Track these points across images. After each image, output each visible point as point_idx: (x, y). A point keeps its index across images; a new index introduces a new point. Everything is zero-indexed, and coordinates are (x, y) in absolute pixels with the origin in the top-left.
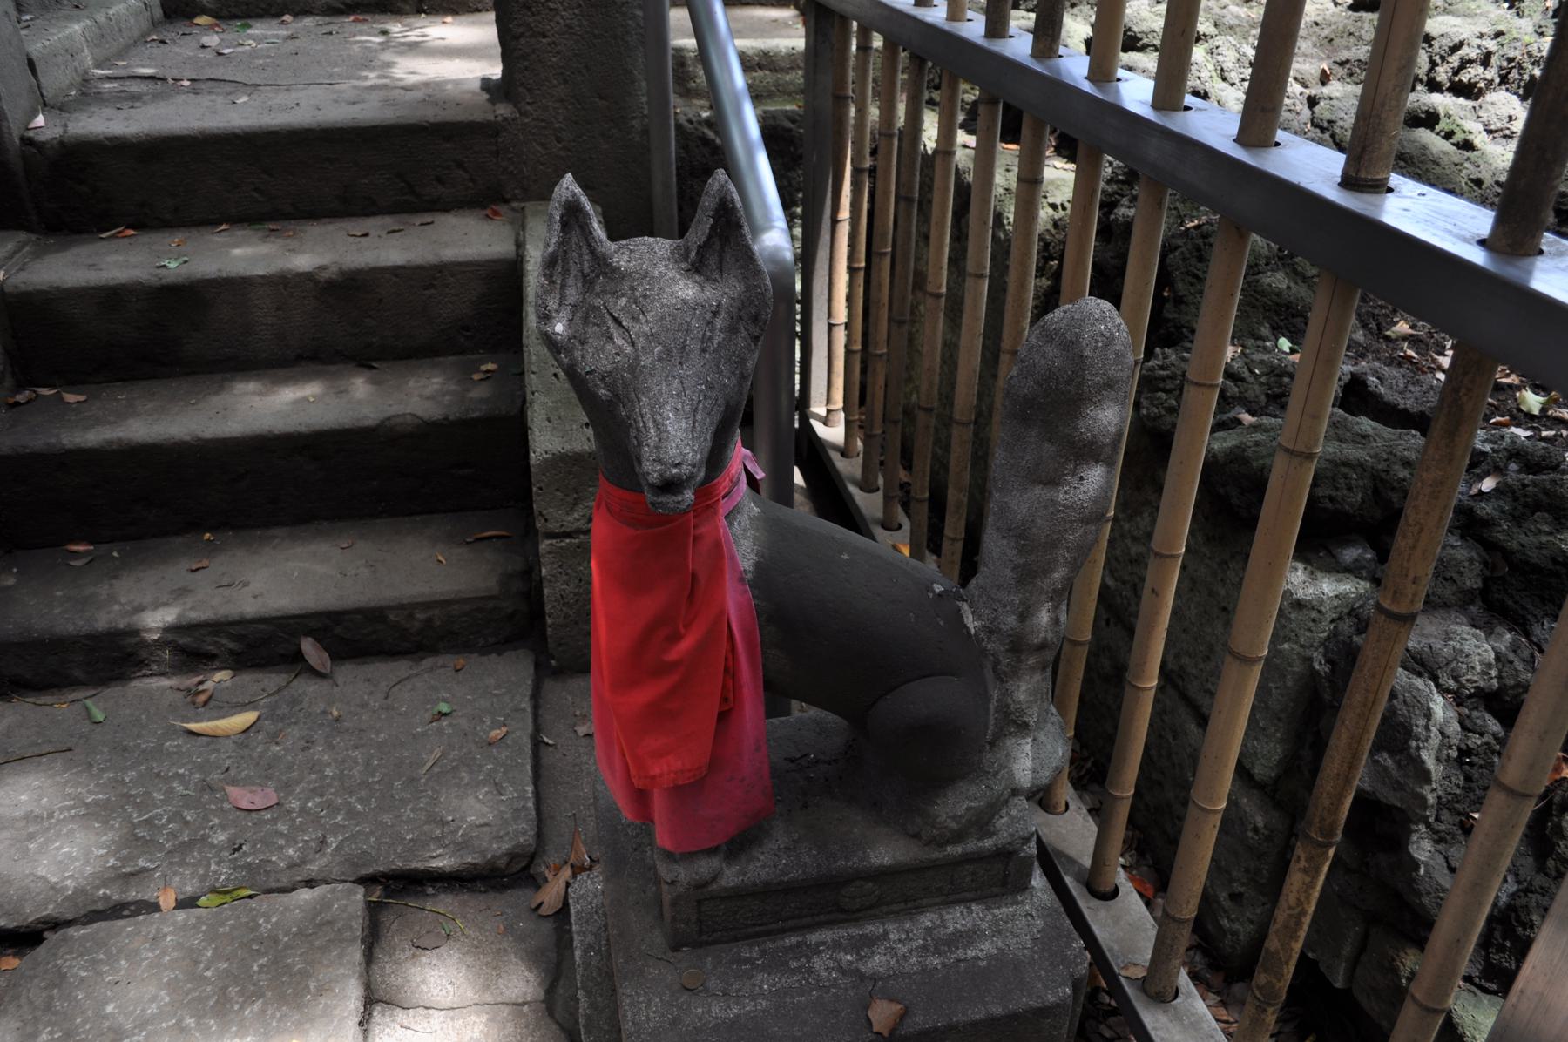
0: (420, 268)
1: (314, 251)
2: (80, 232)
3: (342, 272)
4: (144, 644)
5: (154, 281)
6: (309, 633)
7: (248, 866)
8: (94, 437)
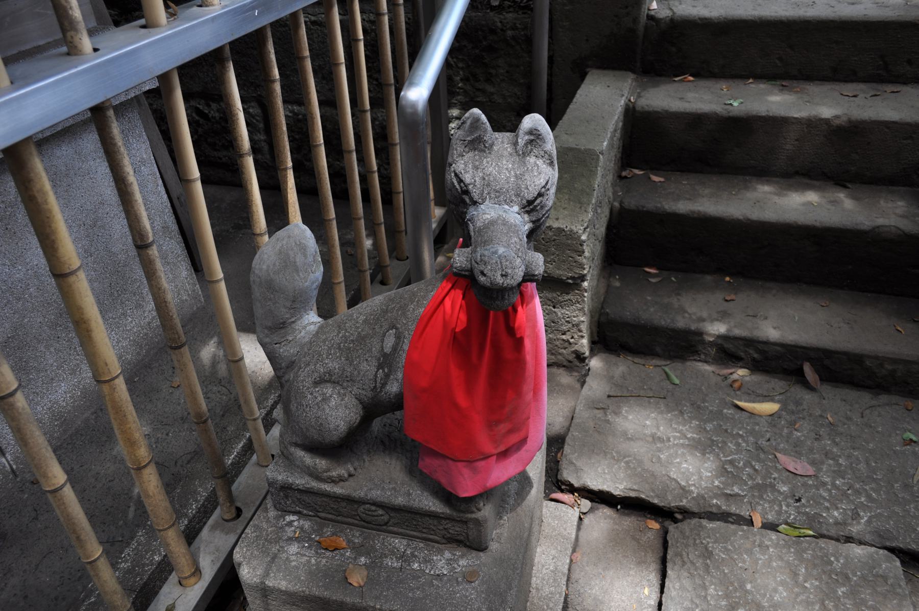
0: (908, 124)
1: (826, 104)
2: (660, 75)
3: (850, 121)
4: (703, 342)
5: (725, 113)
6: (809, 360)
7: (806, 514)
8: (683, 207)
